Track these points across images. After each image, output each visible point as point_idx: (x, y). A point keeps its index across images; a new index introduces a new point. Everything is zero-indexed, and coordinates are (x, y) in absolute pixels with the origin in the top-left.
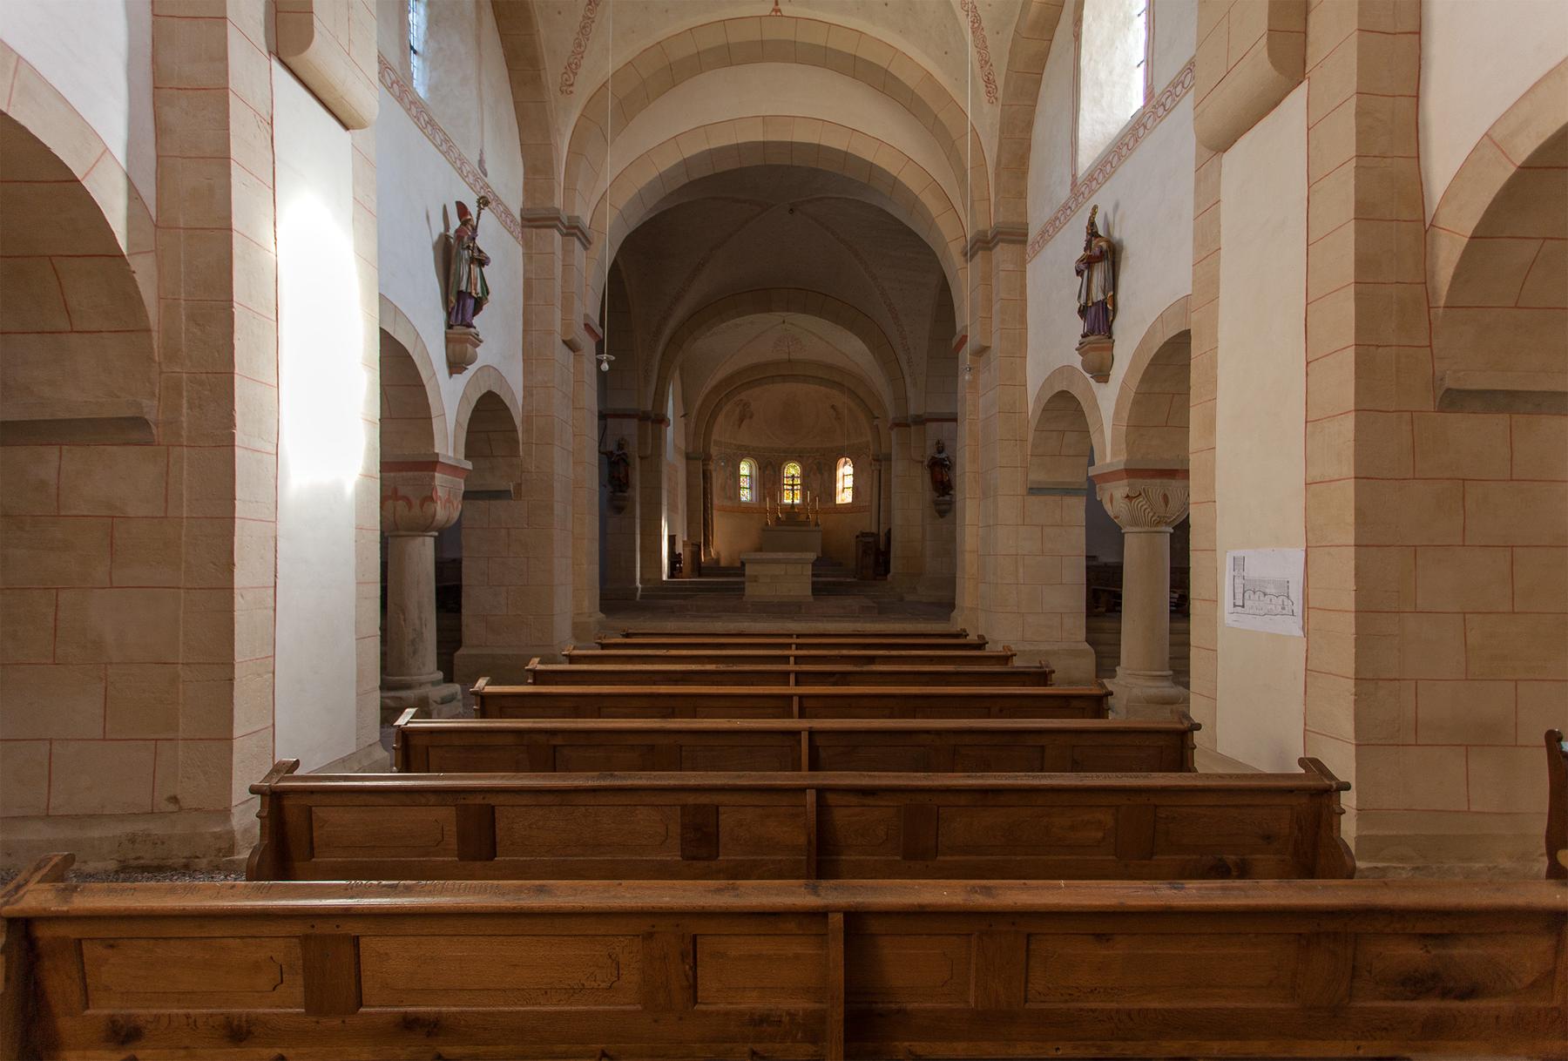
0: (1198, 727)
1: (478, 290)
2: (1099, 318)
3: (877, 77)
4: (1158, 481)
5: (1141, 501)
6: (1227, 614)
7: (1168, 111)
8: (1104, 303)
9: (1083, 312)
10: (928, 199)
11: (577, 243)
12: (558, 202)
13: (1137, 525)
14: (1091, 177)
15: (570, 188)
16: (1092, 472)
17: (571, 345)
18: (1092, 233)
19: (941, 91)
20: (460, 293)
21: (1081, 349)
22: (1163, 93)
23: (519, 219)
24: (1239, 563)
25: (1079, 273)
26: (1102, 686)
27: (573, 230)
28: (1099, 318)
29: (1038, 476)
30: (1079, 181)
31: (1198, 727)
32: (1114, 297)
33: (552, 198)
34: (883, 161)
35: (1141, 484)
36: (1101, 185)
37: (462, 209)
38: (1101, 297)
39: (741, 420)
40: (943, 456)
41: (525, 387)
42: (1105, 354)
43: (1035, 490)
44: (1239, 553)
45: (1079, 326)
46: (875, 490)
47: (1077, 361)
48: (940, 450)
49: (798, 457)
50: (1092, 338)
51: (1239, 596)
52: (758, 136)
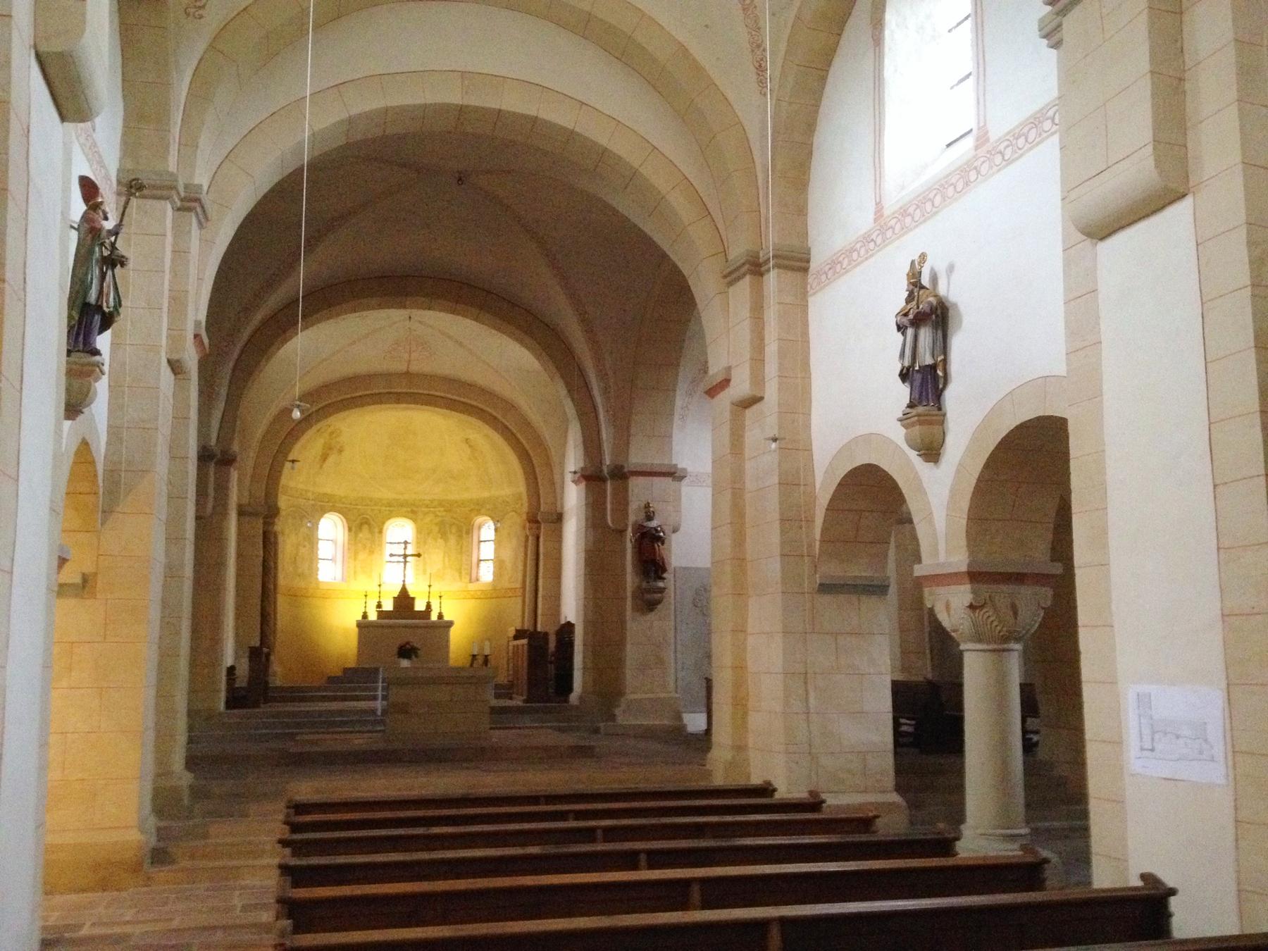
0: (1172, 892)
1: (108, 305)
2: (927, 383)
3: (622, 47)
4: (1004, 588)
5: (988, 611)
6: (1136, 761)
7: (1009, 162)
8: (933, 368)
9: (905, 375)
10: (677, 201)
11: (194, 220)
12: (172, 167)
13: (980, 641)
14: (904, 212)
15: (189, 144)
16: (919, 571)
17: (176, 367)
18: (915, 284)
19: (697, 68)
20: (86, 305)
21: (904, 420)
22: (1000, 141)
23: (114, 180)
24: (1144, 701)
25: (901, 328)
26: (1034, 852)
27: (191, 203)
28: (927, 383)
29: (833, 570)
30: (887, 212)
31: (1172, 892)
32: (945, 361)
33: (164, 158)
34: (620, 147)
35: (985, 589)
36: (918, 224)
37: (89, 188)
38: (929, 361)
39: (324, 458)
40: (654, 524)
41: (109, 426)
42: (936, 429)
43: (826, 588)
44: (1144, 688)
45: (902, 393)
46: (530, 563)
47: (898, 434)
48: (649, 517)
49: (411, 510)
50: (920, 409)
51: (1147, 738)
52: (453, 96)
